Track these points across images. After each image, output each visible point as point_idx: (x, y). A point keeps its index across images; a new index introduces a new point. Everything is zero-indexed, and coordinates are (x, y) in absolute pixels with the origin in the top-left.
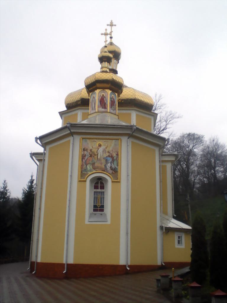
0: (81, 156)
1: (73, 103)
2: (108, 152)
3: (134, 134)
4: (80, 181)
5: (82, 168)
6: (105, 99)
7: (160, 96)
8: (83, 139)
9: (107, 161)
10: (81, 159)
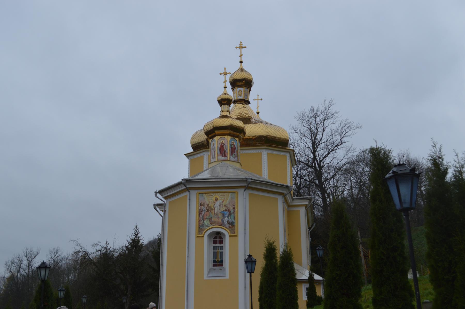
0: (198, 211)
1: (199, 143)
2: (225, 206)
3: (250, 186)
4: (198, 237)
6: (224, 146)
7: (331, 102)
8: (199, 193)
10: (198, 215)
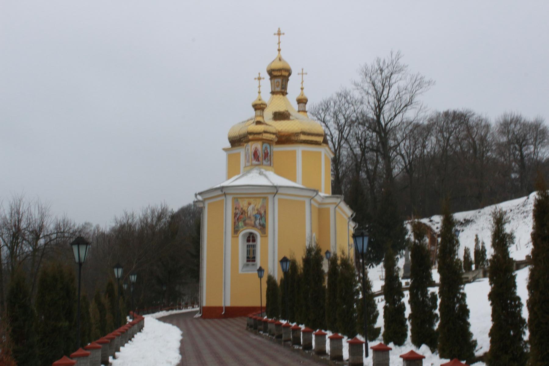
5: (235, 225)
9: (256, 218)
